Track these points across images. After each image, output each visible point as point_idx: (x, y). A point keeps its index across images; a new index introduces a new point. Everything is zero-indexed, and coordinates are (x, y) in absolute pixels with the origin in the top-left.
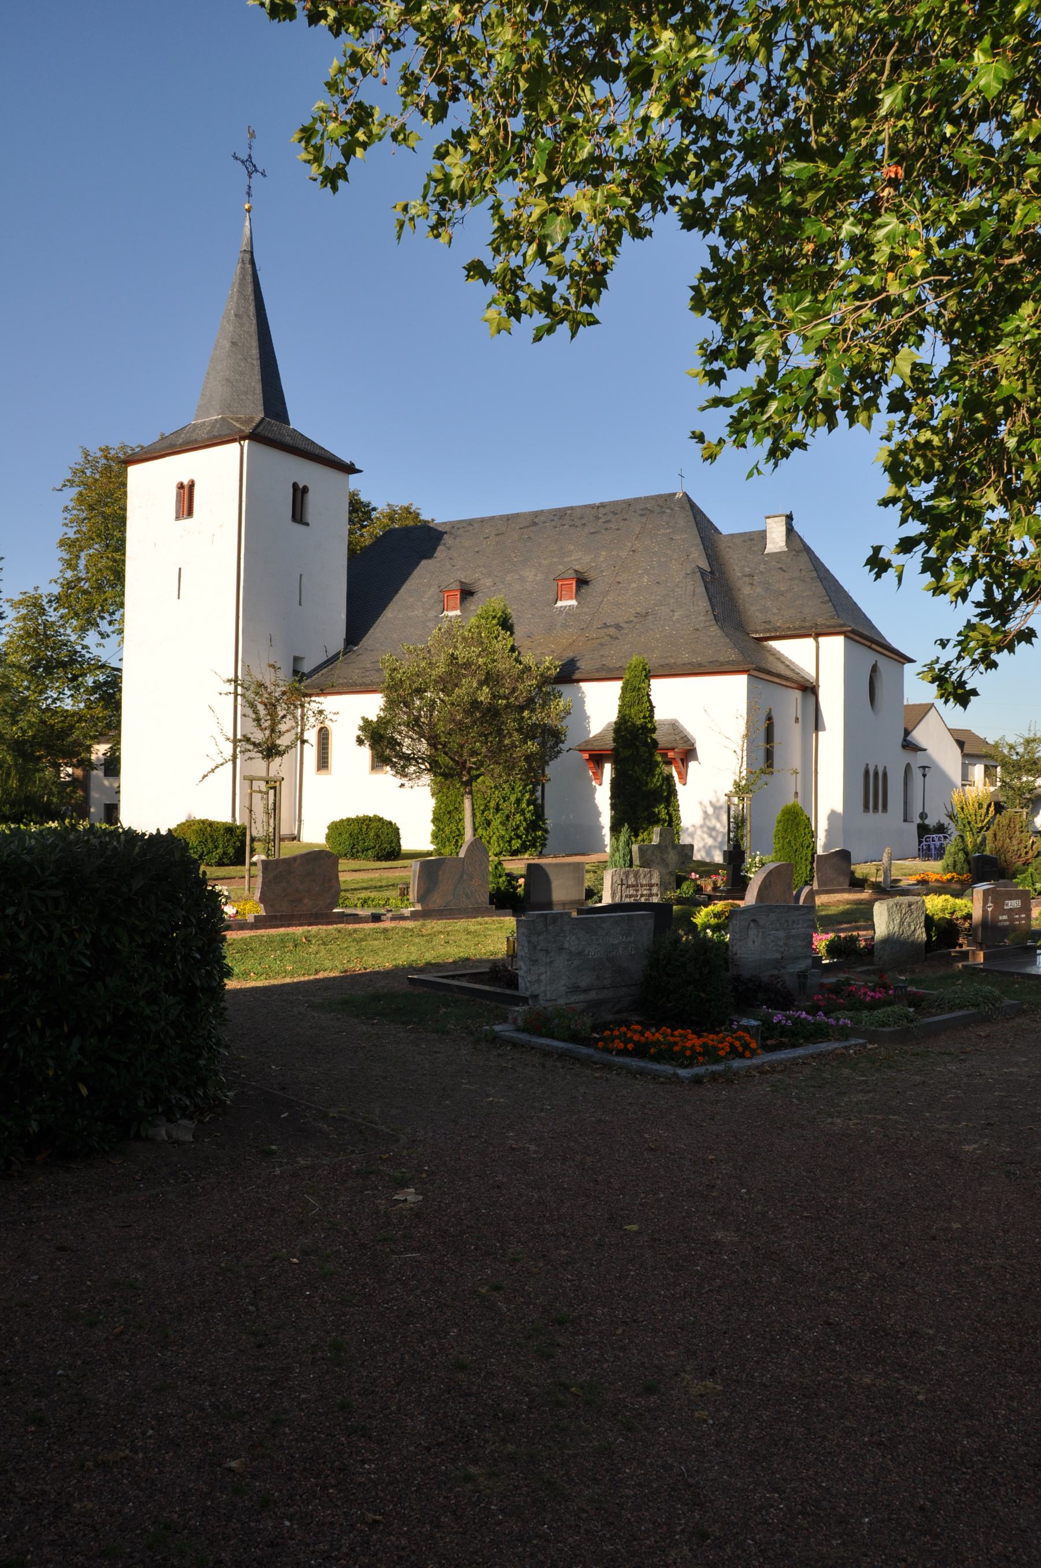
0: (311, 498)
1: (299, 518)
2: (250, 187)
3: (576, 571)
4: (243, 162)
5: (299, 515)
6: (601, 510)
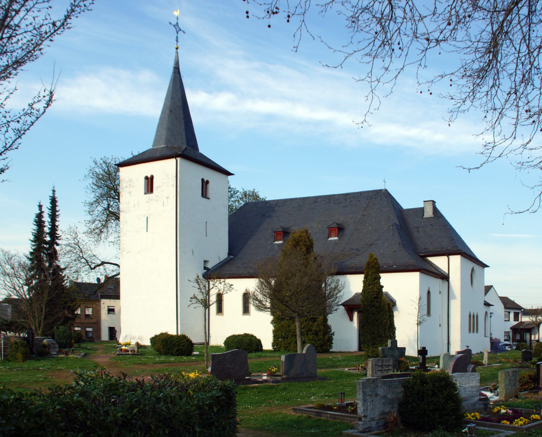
0: (210, 186)
1: (204, 195)
2: (177, 38)
3: (337, 224)
4: (174, 26)
5: (204, 194)
6: (348, 196)
